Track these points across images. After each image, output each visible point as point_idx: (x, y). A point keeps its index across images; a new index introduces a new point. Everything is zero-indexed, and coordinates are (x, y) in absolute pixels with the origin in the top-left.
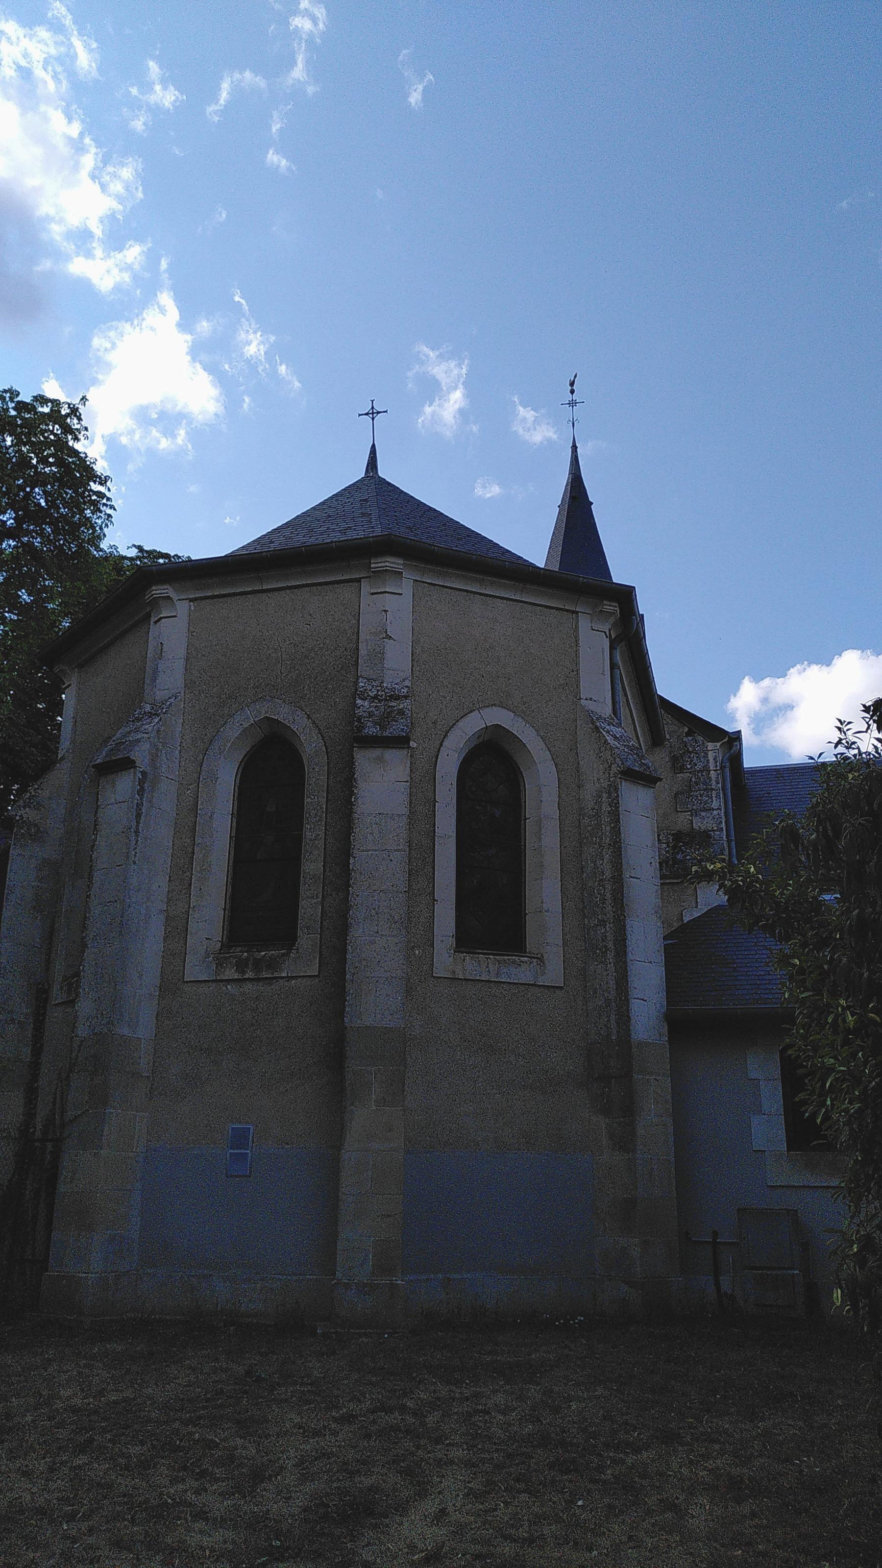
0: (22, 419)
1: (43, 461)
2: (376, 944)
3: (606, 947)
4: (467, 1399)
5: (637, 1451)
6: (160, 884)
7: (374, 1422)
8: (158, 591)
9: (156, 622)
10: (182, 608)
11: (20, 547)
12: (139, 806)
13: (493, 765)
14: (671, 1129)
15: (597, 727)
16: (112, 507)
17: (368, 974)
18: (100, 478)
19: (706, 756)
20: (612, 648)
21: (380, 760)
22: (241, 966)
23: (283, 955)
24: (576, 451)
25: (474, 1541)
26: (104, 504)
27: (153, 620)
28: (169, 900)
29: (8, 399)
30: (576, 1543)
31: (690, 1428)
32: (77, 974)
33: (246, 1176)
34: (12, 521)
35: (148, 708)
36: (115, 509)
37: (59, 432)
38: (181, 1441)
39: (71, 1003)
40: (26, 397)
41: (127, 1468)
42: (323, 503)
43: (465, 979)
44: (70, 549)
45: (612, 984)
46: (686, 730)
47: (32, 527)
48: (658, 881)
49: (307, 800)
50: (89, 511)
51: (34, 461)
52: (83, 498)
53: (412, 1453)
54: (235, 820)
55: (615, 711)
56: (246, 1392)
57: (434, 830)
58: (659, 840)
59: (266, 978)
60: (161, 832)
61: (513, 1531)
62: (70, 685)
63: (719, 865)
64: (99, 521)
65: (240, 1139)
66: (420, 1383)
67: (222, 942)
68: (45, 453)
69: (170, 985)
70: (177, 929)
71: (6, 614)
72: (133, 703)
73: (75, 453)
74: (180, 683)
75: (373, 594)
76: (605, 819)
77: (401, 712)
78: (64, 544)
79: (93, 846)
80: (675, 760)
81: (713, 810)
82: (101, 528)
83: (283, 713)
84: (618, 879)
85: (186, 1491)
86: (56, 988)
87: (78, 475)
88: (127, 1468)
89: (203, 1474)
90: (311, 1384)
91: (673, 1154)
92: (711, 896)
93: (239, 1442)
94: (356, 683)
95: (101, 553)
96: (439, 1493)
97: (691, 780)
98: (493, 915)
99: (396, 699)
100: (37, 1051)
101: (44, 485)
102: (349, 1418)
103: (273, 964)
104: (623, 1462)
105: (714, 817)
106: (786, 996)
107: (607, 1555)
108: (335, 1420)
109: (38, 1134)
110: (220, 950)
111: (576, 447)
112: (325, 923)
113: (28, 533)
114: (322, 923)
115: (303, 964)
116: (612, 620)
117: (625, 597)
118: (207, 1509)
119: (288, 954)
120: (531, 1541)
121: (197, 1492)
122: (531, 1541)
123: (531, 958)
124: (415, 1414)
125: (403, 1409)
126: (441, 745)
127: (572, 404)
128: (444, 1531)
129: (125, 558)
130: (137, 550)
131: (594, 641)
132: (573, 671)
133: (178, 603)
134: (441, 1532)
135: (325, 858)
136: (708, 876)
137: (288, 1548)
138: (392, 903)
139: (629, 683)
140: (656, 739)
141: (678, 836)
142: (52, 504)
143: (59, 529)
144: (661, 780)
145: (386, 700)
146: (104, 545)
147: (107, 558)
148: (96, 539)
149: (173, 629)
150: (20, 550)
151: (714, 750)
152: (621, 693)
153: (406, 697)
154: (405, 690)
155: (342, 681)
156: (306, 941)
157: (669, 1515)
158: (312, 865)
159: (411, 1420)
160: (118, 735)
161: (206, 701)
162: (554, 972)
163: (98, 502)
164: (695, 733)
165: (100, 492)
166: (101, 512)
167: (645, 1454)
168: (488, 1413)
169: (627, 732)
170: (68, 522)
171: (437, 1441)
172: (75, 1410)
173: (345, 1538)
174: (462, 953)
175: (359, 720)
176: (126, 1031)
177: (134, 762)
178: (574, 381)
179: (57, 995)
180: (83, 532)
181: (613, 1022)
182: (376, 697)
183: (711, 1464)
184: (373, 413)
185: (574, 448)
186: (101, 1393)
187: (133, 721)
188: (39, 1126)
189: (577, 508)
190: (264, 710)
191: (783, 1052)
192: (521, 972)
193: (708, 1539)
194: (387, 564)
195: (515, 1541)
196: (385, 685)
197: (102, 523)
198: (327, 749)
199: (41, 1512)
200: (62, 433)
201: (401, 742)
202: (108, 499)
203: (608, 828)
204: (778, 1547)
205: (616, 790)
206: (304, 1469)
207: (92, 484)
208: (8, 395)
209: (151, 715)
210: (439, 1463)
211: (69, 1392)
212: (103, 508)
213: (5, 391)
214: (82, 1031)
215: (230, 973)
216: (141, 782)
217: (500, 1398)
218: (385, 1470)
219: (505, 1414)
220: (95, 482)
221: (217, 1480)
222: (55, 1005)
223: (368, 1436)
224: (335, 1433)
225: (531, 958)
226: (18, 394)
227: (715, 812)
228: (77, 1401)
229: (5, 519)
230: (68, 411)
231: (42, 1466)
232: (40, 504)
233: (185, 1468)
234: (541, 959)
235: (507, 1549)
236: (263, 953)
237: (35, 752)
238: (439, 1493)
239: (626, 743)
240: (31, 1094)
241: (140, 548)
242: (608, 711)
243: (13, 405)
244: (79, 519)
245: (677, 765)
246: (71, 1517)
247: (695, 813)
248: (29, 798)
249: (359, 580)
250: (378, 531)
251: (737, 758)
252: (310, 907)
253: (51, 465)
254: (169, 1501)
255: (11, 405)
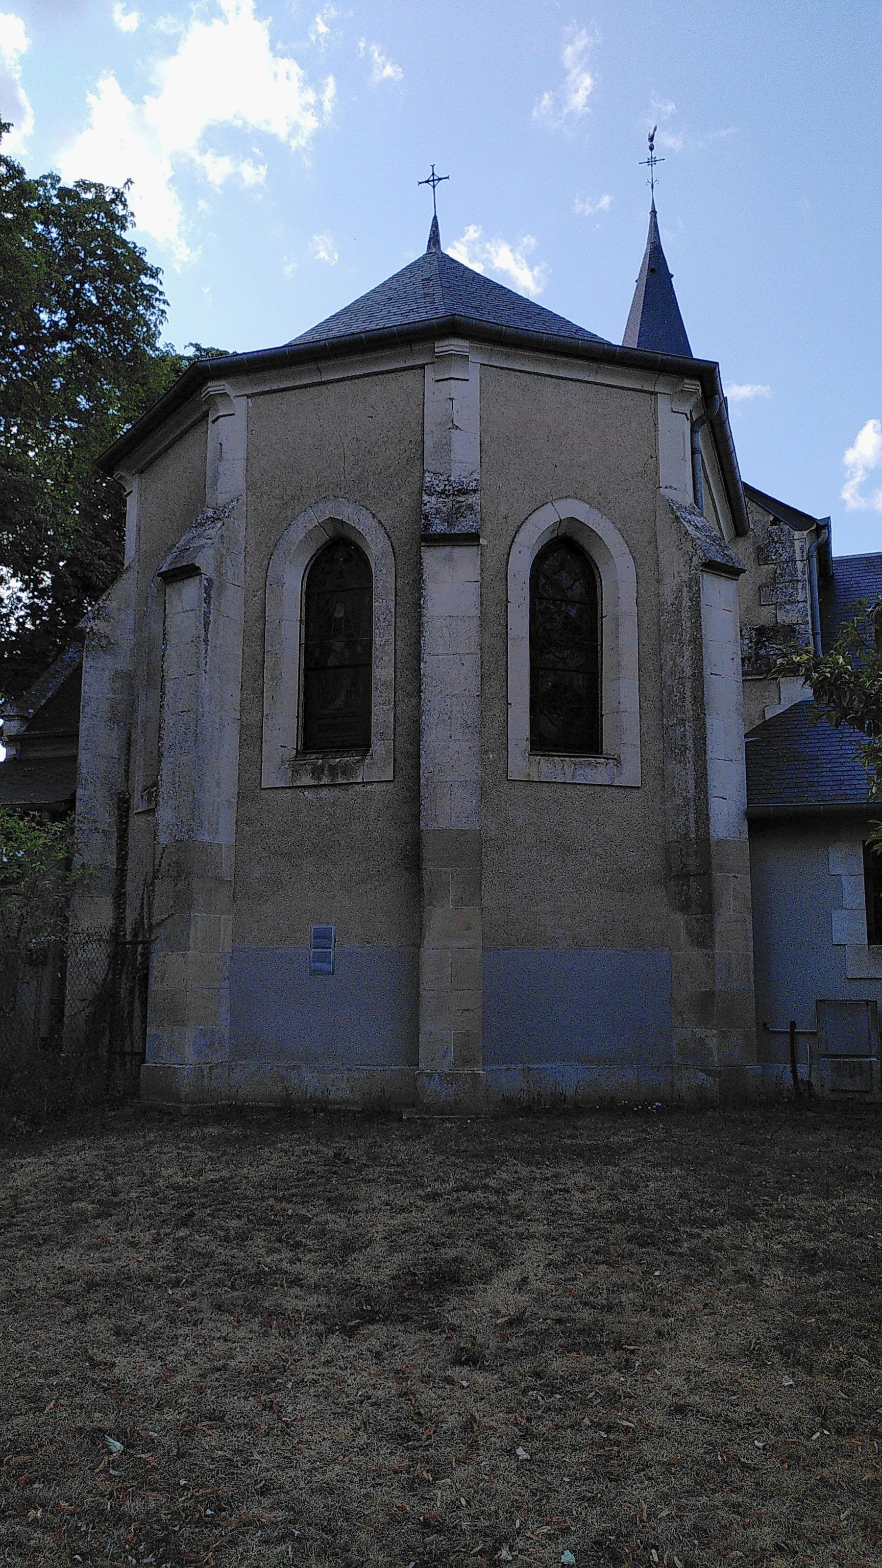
0: (67, 207)
1: (91, 253)
2: (449, 749)
3: (685, 746)
4: (548, 1179)
5: (713, 1226)
6: (233, 695)
7: (458, 1199)
8: (214, 387)
9: (213, 422)
10: (240, 406)
11: (74, 349)
12: (207, 615)
13: (567, 560)
14: (750, 927)
15: (677, 518)
16: (165, 302)
17: (442, 779)
18: (151, 270)
19: (792, 546)
20: (693, 431)
21: (449, 559)
22: (317, 772)
23: (358, 761)
24: (655, 217)
25: (556, 1307)
26: (157, 299)
27: (211, 419)
28: (242, 710)
29: (49, 186)
30: (653, 1310)
31: (764, 1205)
32: (156, 784)
33: (329, 974)
34: (64, 322)
35: (210, 512)
36: (168, 304)
37: (104, 221)
38: (276, 1215)
39: (151, 811)
40: (68, 182)
41: (227, 1239)
42: (383, 285)
43: (541, 782)
44: (125, 349)
45: (691, 783)
46: (772, 518)
47: (84, 328)
48: (741, 679)
49: (375, 604)
50: (141, 307)
51: (82, 255)
52: (134, 293)
53: (495, 1229)
54: (303, 627)
55: (696, 501)
56: (335, 1173)
57: (507, 632)
58: (741, 635)
59: (342, 784)
60: (229, 639)
61: (592, 1299)
62: (131, 492)
63: (805, 657)
64: (153, 318)
65: (322, 939)
66: (501, 1164)
67: (297, 749)
68: (93, 245)
69: (248, 792)
70: (252, 737)
71: (66, 422)
72: (197, 511)
73: (124, 243)
74: (242, 485)
75: (437, 381)
76: (685, 614)
77: (470, 507)
78: (119, 344)
79: (163, 656)
80: (759, 550)
81: (798, 602)
82: (155, 326)
83: (348, 513)
84: (698, 676)
85: (282, 1260)
86: (137, 795)
87: (128, 268)
88: (227, 1239)
89: (298, 1245)
90: (398, 1165)
91: (751, 949)
92: (796, 691)
93: (330, 1217)
94: (423, 478)
95: (157, 353)
96: (522, 1263)
97: (776, 572)
98: (568, 717)
99: (464, 494)
100: (122, 859)
101: (93, 280)
102: (434, 1196)
103: (346, 770)
104: (699, 1236)
105: (799, 609)
106: (874, 790)
107: (683, 1321)
108: (421, 1198)
109: (129, 938)
110: (296, 757)
111: (656, 212)
112: (398, 729)
113: (81, 333)
114: (395, 729)
115: (378, 767)
116: (694, 400)
117: (707, 375)
118: (301, 1277)
119: (363, 760)
120: (609, 1308)
121: (292, 1262)
122: (609, 1308)
123: (608, 759)
124: (497, 1192)
125: (486, 1187)
126: (513, 541)
127: (652, 162)
128: (526, 1297)
129: (182, 358)
130: (194, 349)
131: (673, 422)
132: (652, 457)
133: (235, 400)
134: (523, 1299)
135: (395, 663)
136: (792, 670)
137: (378, 1312)
138: (465, 708)
139: (712, 469)
140: (740, 529)
141: (761, 631)
142: (104, 301)
143: (114, 329)
144: (744, 571)
145: (454, 495)
146: (160, 343)
147: (163, 358)
148: (151, 338)
149: (231, 425)
150: (75, 352)
151: (801, 539)
152: (703, 480)
153: (475, 491)
154: (474, 484)
155: (408, 476)
156: (380, 747)
157: (744, 1285)
158: (383, 671)
159: (493, 1198)
160: (182, 542)
161: (269, 502)
162: (631, 772)
163: (151, 297)
164: (780, 521)
165: (153, 286)
166: (154, 307)
167: (721, 1229)
168: (567, 1191)
169: (713, 518)
170: (121, 321)
171: (519, 1218)
172: (176, 1188)
173: (432, 1303)
174: (537, 755)
175: (426, 518)
176: (206, 838)
177: (199, 568)
178: (653, 135)
179: (138, 804)
180: (137, 330)
181: (692, 821)
182: (443, 492)
183: (784, 1238)
184: (433, 180)
185: (654, 213)
186: (200, 1172)
187: (196, 527)
188: (129, 930)
189: (656, 277)
190: (328, 510)
191: (867, 849)
192: (596, 772)
193: (782, 1307)
194: (452, 348)
195: (594, 1307)
196: (452, 479)
197: (156, 320)
198: (393, 550)
199: (148, 1279)
200: (107, 222)
201: (471, 539)
202: (161, 293)
203: (689, 624)
204: (852, 1316)
205: (697, 582)
206: (392, 1242)
207: (142, 277)
208: (49, 181)
209: (214, 520)
210: (521, 1236)
211: (170, 1171)
212: (157, 304)
213: (45, 177)
214: (163, 839)
215: (306, 780)
216: (207, 590)
217: (580, 1179)
218: (469, 1243)
219: (583, 1192)
220: (146, 275)
221: (310, 1250)
222: (136, 814)
223: (452, 1212)
224: (421, 1210)
225: (608, 759)
226: (59, 180)
227: (801, 605)
228: (179, 1180)
229: (56, 319)
230: (113, 196)
231: (147, 1237)
232: (91, 301)
233: (280, 1241)
234: (618, 761)
235: (586, 1315)
236: (338, 760)
237: (104, 564)
238: (522, 1263)
239: (708, 533)
240: (119, 898)
241: (198, 347)
242: (689, 499)
243: (55, 192)
244: (133, 316)
245: (762, 555)
246: (176, 1284)
247: (778, 606)
248: (97, 610)
249: (422, 367)
250: (442, 313)
251: (824, 548)
252: (382, 714)
253: (100, 258)
254: (266, 1269)
255: (54, 192)
